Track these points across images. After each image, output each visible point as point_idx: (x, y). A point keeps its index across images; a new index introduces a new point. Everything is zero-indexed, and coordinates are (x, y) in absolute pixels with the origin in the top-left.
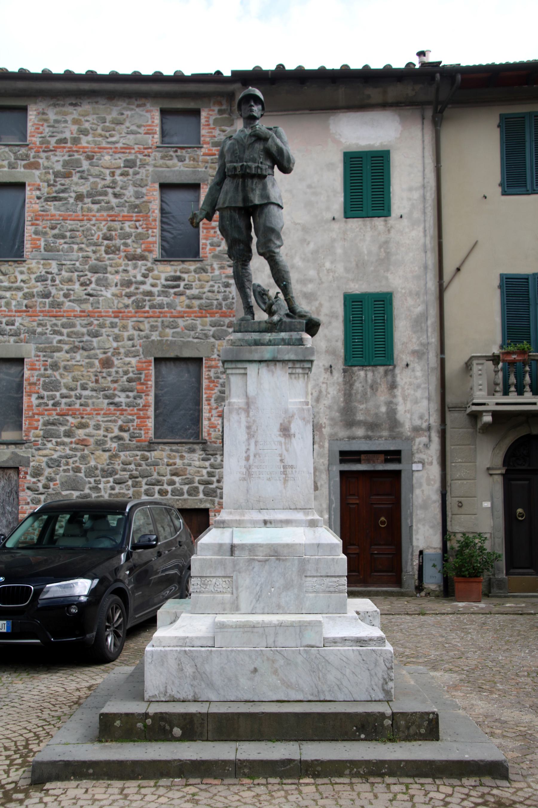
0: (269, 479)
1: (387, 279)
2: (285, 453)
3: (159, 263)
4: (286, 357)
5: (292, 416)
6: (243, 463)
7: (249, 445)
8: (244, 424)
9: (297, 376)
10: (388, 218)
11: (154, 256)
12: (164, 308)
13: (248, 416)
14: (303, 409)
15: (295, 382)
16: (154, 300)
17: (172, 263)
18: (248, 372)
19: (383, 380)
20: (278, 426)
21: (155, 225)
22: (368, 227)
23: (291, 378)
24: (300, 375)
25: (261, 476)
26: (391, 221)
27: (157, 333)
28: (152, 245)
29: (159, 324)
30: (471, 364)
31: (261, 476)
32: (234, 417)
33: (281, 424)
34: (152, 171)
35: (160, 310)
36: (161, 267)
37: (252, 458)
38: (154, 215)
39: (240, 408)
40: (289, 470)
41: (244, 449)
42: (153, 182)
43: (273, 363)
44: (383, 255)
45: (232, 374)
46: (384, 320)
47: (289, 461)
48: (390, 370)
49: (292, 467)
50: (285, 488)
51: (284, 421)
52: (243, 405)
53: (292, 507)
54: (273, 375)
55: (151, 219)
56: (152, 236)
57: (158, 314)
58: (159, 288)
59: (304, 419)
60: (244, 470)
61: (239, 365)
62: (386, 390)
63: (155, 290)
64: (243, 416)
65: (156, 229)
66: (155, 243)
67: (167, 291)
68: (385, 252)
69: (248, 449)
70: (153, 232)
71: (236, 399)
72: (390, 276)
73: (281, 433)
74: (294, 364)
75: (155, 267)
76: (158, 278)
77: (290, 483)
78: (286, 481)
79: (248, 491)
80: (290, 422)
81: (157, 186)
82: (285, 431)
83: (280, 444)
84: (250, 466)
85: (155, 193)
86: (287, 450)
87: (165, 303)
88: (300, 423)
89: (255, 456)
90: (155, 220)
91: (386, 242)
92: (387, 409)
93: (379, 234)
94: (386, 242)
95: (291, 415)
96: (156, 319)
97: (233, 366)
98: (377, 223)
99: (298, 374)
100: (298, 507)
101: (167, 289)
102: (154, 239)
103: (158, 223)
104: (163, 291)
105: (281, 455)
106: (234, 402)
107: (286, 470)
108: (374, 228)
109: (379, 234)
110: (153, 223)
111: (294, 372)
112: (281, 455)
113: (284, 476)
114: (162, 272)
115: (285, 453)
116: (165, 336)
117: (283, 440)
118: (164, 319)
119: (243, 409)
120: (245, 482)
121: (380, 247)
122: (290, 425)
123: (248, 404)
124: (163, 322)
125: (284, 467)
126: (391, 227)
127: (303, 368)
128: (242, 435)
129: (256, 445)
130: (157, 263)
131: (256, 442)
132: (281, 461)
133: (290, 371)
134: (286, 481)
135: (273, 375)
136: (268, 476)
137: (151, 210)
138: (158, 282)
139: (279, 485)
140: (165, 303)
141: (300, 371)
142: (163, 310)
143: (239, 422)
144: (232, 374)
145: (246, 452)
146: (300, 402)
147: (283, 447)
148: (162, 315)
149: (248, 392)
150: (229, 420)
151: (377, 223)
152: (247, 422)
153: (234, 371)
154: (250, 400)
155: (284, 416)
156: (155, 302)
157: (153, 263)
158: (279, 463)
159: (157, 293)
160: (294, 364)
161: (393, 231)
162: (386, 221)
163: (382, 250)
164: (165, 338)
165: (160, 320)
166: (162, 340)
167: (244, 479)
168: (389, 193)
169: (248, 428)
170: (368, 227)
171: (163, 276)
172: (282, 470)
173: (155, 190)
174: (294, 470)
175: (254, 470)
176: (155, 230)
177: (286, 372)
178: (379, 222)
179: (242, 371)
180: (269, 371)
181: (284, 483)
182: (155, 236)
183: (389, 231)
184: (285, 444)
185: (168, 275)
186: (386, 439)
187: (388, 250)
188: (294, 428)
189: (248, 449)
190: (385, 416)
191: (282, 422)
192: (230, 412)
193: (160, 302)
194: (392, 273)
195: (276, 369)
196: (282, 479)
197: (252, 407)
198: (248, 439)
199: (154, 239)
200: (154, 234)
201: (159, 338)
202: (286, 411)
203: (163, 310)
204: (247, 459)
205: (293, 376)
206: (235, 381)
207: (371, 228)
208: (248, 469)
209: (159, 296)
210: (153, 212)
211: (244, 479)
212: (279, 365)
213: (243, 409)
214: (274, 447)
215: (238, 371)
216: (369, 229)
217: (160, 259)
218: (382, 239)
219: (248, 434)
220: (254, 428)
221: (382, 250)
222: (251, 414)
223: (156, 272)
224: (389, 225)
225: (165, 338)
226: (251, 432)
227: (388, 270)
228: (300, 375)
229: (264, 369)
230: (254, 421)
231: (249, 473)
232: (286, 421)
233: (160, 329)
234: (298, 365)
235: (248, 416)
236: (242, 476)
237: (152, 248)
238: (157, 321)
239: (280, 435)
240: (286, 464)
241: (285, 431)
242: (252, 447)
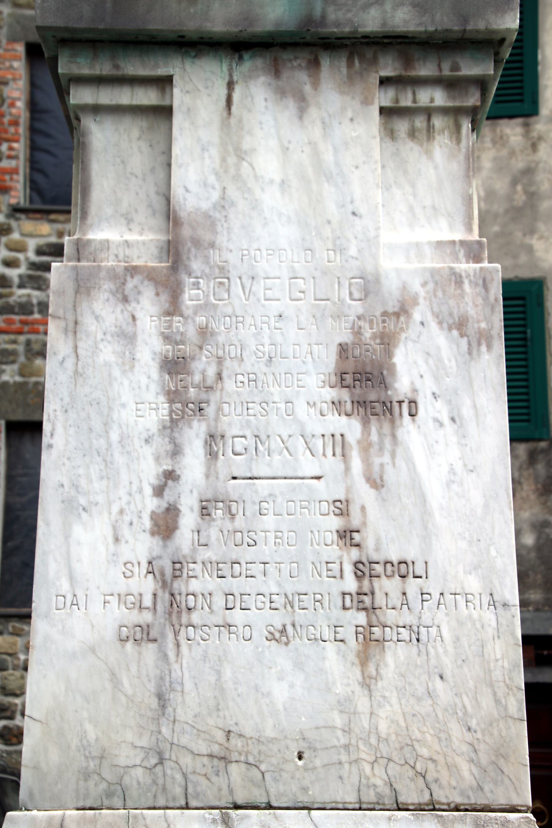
0: (280, 636)
1: (530, 250)
2: (364, 494)
3: (23, 216)
4: (371, 22)
5: (403, 311)
6: (142, 545)
7: (176, 452)
8: (150, 346)
9: (420, 122)
10: (532, 120)
11: (13, 201)
12: (32, 313)
13: (173, 308)
14: (458, 279)
15: (411, 150)
16: (11, 295)
17: (53, 217)
18: (179, 97)
19: (525, 473)
20: (329, 360)
21: (17, 132)
22: (488, 139)
23: (390, 134)
24: (438, 122)
25: (237, 617)
26: (539, 126)
27: (15, 367)
28: (7, 177)
29: (21, 348)
30: (242, 739)
31: (237, 617)
32: (102, 313)
33: (343, 349)
34: (10, 15)
35: (23, 317)
36: (28, 225)
37: (188, 520)
38: (14, 111)
39: (133, 271)
40: (388, 587)
41: (150, 471)
42: (12, 39)
43: (304, 56)
44: (520, 198)
45: (97, 110)
46: (525, 339)
47: (386, 538)
48: (543, 451)
49: (402, 569)
50: (367, 683)
51: (357, 333)
52: (147, 257)
53: (410, 796)
54: (302, 111)
55: (6, 120)
56: (10, 157)
57: (18, 325)
58: (22, 270)
59: (460, 325)
60: (147, 586)
61: (134, 67)
62: (533, 497)
63: (14, 274)
64: (147, 308)
65: (17, 141)
66: (15, 171)
67: (39, 277)
68: (526, 192)
69: (170, 476)
70: (11, 149)
71: (114, 225)
72: (536, 243)
73: (345, 395)
74: (408, 62)
75: (14, 224)
76: (22, 249)
77: (395, 658)
78: (370, 643)
79: (162, 699)
80: (387, 341)
81: (20, 48)
82: (366, 384)
83: (340, 445)
84: (178, 565)
85: (16, 64)
86: (376, 483)
87: (35, 301)
88: (442, 342)
89: (205, 512)
90: (15, 123)
91: (529, 171)
92: (538, 538)
93: (512, 153)
94: (529, 171)
95: (392, 306)
96: (12, 337)
97: (104, 68)
98: (508, 131)
99: (429, 112)
100: (442, 796)
101: (39, 273)
102: (13, 163)
103: (22, 130)
104: (30, 277)
105: (342, 508)
106: (106, 244)
107: (373, 586)
108: (500, 141)
109: (512, 153)
110: (12, 130)
111: (406, 101)
112: (342, 508)
113: (361, 618)
114: (31, 235)
115: (364, 494)
116: (31, 375)
117: (352, 428)
118: (33, 337)
119: (150, 275)
120: (150, 650)
121: (514, 182)
122: (389, 353)
123: (174, 252)
124: (28, 343)
125: (362, 570)
126: (540, 138)
127: (451, 84)
128: (138, 399)
129: (212, 455)
130: (18, 215)
131: (213, 439)
132: (347, 536)
133: (386, 97)
134: (370, 643)
135: (302, 111)
136: (277, 620)
137: (8, 101)
138: (21, 256)
139: (337, 664)
140: (35, 301)
141: (438, 97)
142: (31, 318)
143: (127, 337)
144: (97, 110)
145: (159, 491)
146: (440, 244)
147: (356, 463)
148: (26, 329)
149: (177, 190)
150: (74, 329)
151: (508, 131)
152: (167, 338)
153: (107, 96)
154: (186, 232)
155: (357, 308)
156: (11, 300)
157: (8, 216)
158: (333, 552)
159: (16, 280)
160: (408, 62)
161: (543, 148)
162: (526, 125)
163: (519, 188)
164: (33, 379)
165: (22, 338)
166: (25, 384)
167: (145, 635)
168: (535, 63)
169: (174, 366)
170: (488, 139)
171: (32, 244)
172: (350, 584)
173: (16, 58)
174: (413, 586)
175: (201, 583)
176: (15, 145)
177: (367, 102)
178: (512, 131)
179: (147, 97)
180: (281, 93)
181: (364, 659)
182: (16, 157)
183: (534, 147)
184: (365, 447)
185: (42, 241)
186: (537, 610)
187: (533, 189)
188: (409, 369)
189: (170, 476)
190: (533, 555)
191: (346, 337)
192: (83, 286)
193: (24, 299)
194: (541, 237)
195: (316, 85)
196: (348, 633)
197: (196, 265)
198: (173, 425)
199: (13, 163)
200: (13, 153)
201: (18, 379)
202: (368, 286)
203: (31, 318)
204: (165, 524)
205: (402, 126)
206: (111, 152)
207: (494, 142)
208: (169, 576)
209: (21, 286)
210: (12, 105)
211: (145, 635)
212: (332, 69)
213: (150, 275)
214: (308, 466)
215: (125, 96)
216: (488, 143)
217: (28, 205)
218: (519, 164)
219: (173, 396)
220: (203, 367)
221: (519, 188)
222: (189, 297)
223: (16, 236)
224: (535, 134)
225: (33, 379)
226: (186, 384)
227: (532, 231)
228: (438, 122)
229: (257, 94)
230: (204, 332)
231: (169, 606)
232: (368, 334)
233: (22, 359)
234: (425, 69)
235: (173, 308)
236: (135, 617)
237: (9, 183)
238: (14, 342)
239: (337, 405)
240: (370, 550)
241: (366, 384)
242: (193, 466)
